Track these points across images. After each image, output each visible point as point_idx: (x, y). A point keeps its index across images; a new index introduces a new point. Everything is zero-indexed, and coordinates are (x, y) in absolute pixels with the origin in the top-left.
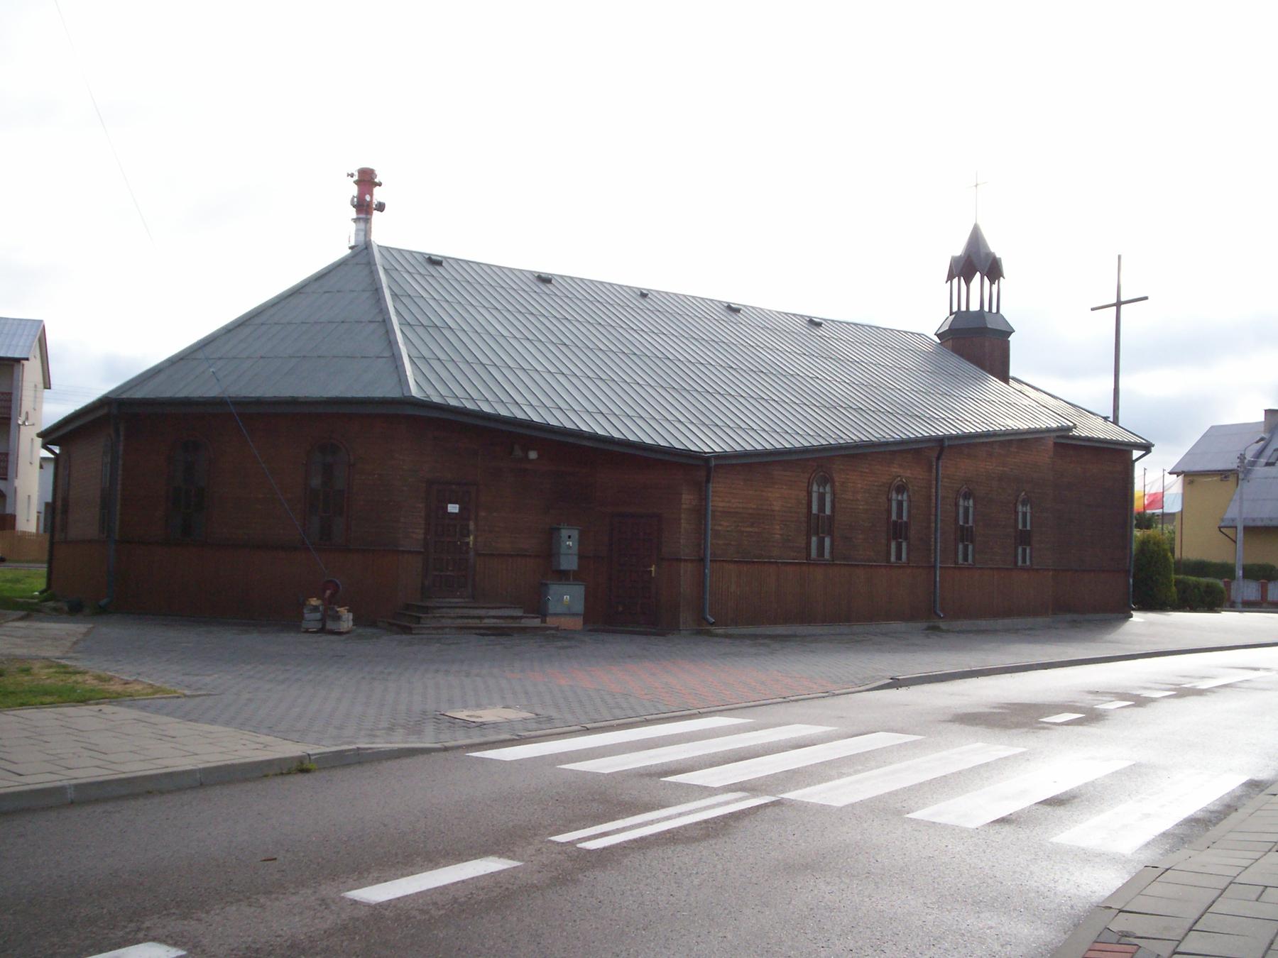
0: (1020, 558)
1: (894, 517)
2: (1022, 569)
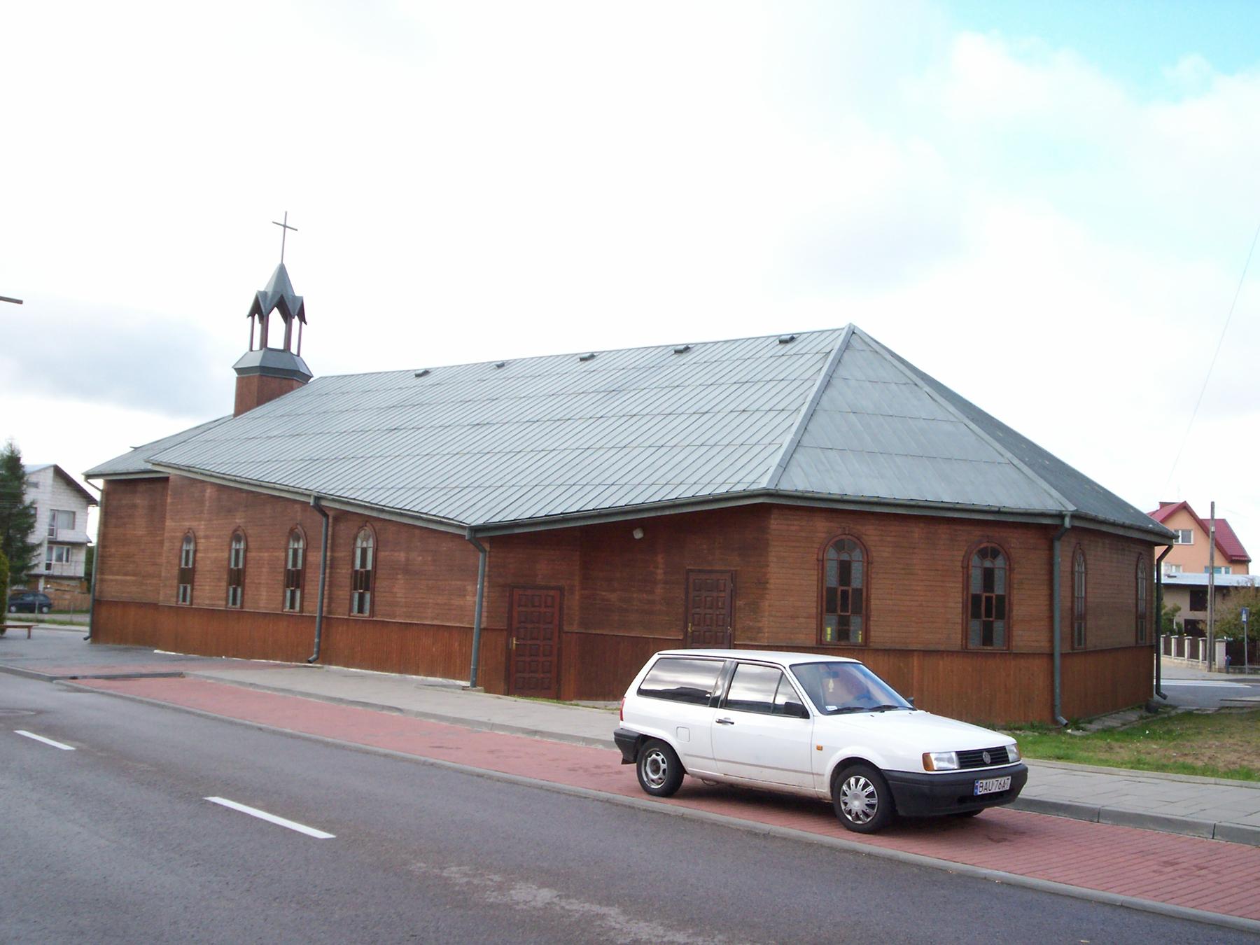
0: (288, 604)
1: (232, 566)
2: (290, 616)
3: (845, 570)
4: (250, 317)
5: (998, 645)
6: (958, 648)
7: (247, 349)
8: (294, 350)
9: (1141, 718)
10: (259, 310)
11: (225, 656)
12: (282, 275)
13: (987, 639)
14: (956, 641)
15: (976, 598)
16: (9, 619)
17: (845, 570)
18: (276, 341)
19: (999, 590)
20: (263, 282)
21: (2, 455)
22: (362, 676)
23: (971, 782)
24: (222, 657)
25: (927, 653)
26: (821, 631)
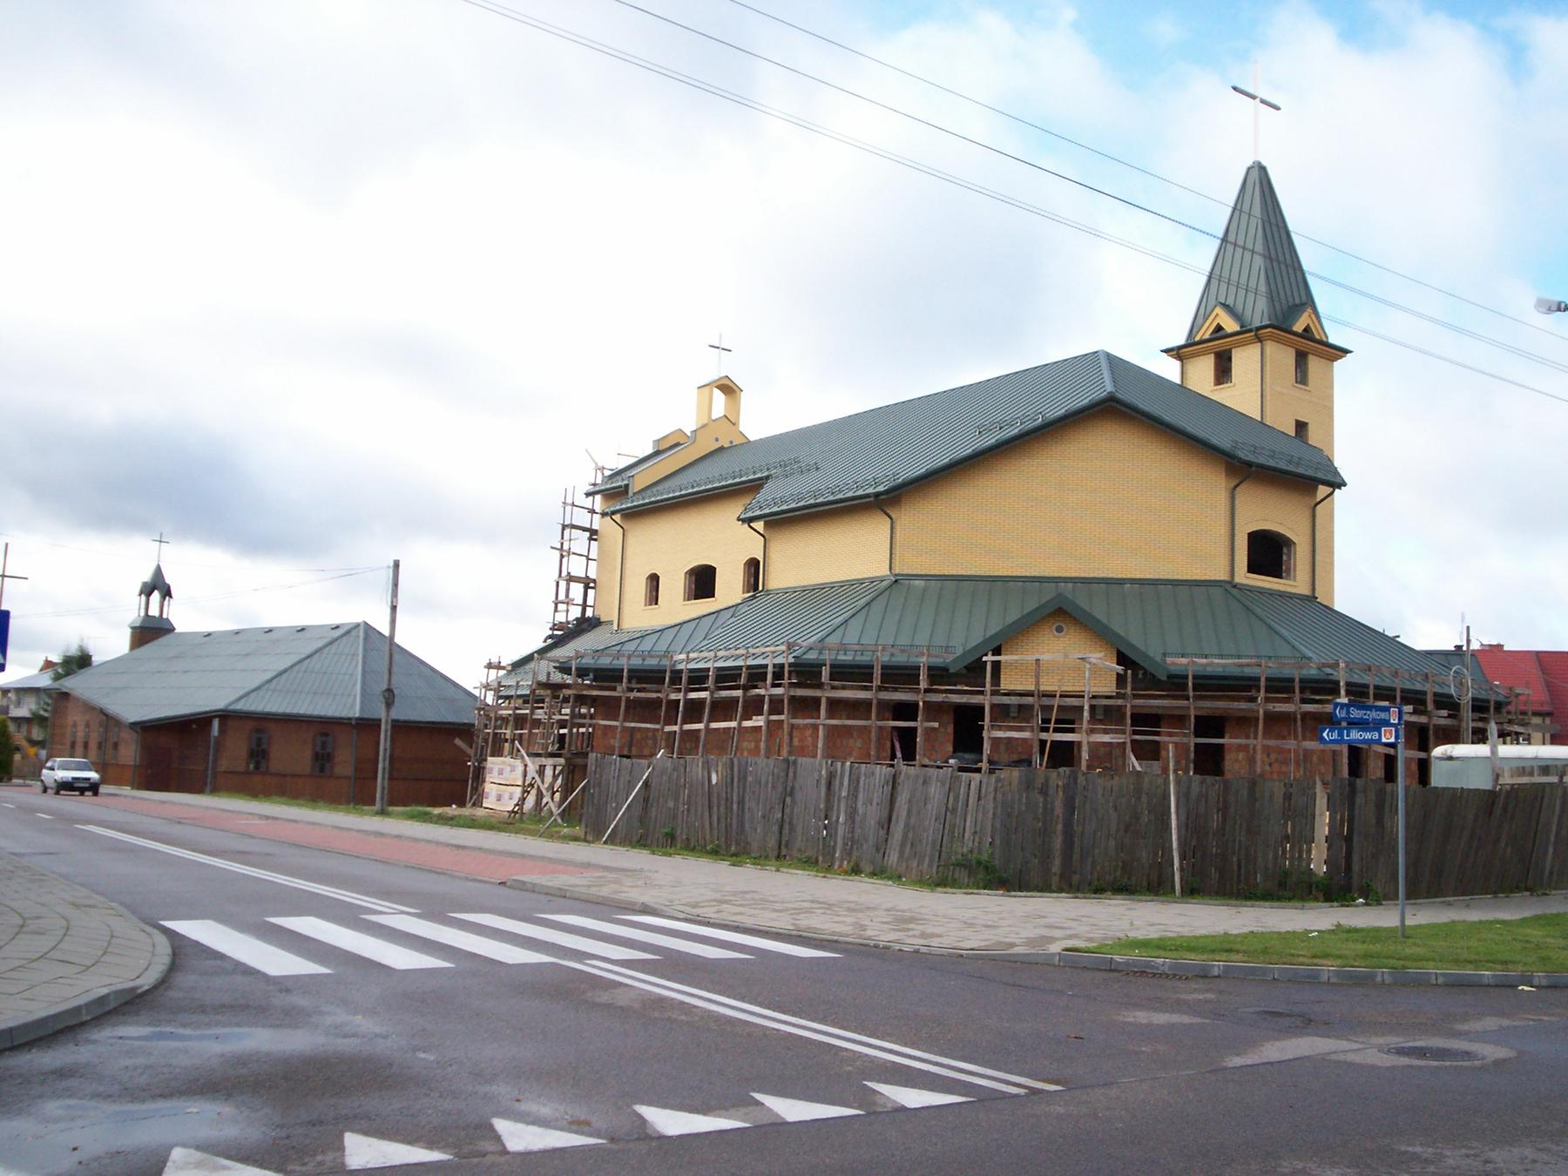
3: (324, 744)
4: (143, 597)
5: (262, 769)
6: (243, 771)
7: (137, 615)
8: (165, 616)
9: (670, 808)
10: (147, 590)
11: (456, 804)
12: (158, 572)
13: (322, 770)
14: (308, 770)
15: (263, 757)
16: (1301, 300)
17: (324, 744)
18: (154, 611)
19: (329, 750)
20: (147, 576)
21: (2, 706)
22: (1480, 898)
23: (74, 783)
24: (451, 806)
25: (294, 776)
26: (248, 766)
